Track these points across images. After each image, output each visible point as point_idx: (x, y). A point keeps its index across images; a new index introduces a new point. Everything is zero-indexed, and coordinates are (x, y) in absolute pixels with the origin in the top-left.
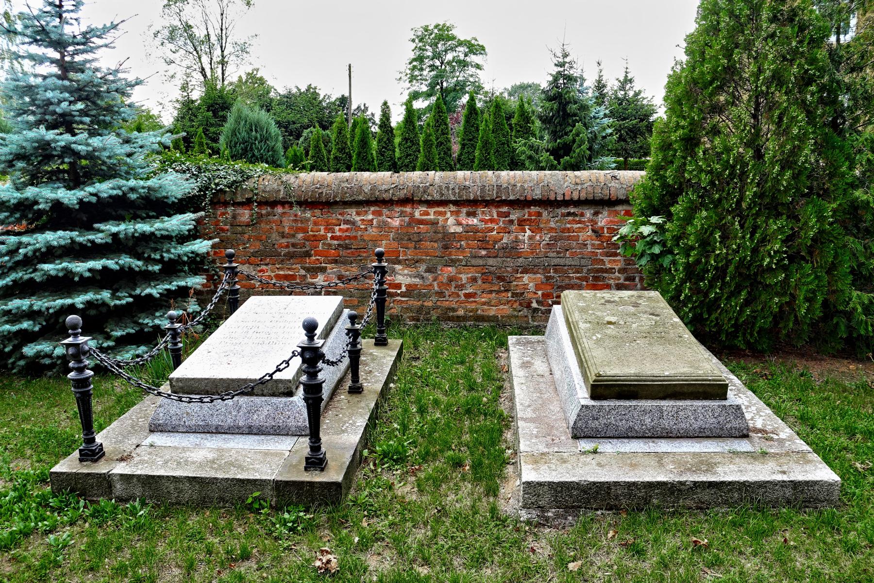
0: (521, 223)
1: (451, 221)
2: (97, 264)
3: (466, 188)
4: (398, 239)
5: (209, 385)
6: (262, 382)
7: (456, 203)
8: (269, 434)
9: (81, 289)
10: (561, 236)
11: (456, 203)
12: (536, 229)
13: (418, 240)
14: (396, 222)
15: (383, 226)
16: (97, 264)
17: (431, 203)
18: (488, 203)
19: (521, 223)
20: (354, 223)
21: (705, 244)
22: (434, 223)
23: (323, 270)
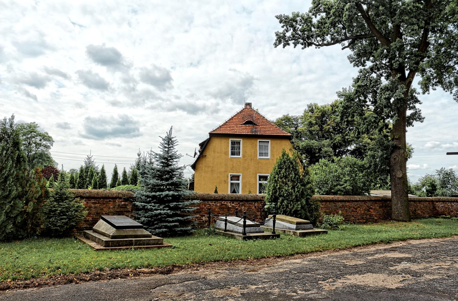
0: (242, 205)
1: (229, 204)
2: (173, 224)
3: (232, 197)
4: (219, 208)
5: (399, 159)
6: (235, 223)
7: (231, 201)
8: (416, 239)
9: (122, 135)
10: (249, 208)
11: (231, 201)
12: (245, 206)
13: (223, 208)
14: (219, 205)
15: (216, 206)
16: (173, 224)
17: (225, 200)
18: (237, 201)
19: (242, 205)
20: (210, 205)
21: (287, 206)
22: (226, 205)
23: (204, 216)
